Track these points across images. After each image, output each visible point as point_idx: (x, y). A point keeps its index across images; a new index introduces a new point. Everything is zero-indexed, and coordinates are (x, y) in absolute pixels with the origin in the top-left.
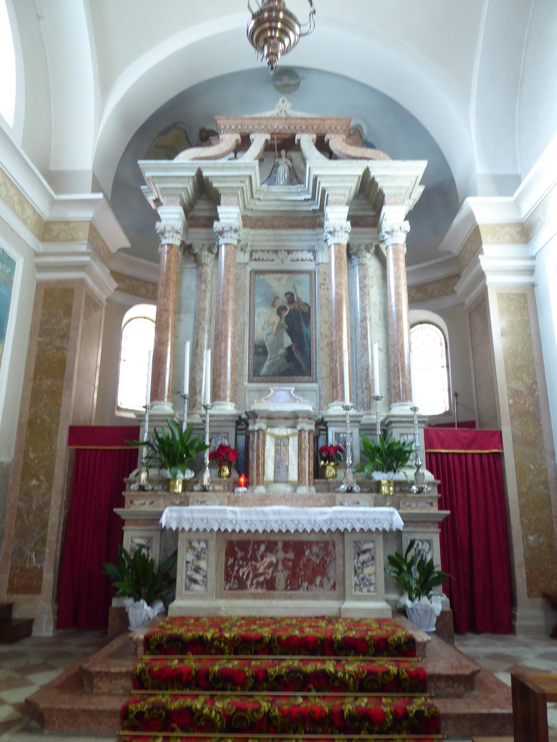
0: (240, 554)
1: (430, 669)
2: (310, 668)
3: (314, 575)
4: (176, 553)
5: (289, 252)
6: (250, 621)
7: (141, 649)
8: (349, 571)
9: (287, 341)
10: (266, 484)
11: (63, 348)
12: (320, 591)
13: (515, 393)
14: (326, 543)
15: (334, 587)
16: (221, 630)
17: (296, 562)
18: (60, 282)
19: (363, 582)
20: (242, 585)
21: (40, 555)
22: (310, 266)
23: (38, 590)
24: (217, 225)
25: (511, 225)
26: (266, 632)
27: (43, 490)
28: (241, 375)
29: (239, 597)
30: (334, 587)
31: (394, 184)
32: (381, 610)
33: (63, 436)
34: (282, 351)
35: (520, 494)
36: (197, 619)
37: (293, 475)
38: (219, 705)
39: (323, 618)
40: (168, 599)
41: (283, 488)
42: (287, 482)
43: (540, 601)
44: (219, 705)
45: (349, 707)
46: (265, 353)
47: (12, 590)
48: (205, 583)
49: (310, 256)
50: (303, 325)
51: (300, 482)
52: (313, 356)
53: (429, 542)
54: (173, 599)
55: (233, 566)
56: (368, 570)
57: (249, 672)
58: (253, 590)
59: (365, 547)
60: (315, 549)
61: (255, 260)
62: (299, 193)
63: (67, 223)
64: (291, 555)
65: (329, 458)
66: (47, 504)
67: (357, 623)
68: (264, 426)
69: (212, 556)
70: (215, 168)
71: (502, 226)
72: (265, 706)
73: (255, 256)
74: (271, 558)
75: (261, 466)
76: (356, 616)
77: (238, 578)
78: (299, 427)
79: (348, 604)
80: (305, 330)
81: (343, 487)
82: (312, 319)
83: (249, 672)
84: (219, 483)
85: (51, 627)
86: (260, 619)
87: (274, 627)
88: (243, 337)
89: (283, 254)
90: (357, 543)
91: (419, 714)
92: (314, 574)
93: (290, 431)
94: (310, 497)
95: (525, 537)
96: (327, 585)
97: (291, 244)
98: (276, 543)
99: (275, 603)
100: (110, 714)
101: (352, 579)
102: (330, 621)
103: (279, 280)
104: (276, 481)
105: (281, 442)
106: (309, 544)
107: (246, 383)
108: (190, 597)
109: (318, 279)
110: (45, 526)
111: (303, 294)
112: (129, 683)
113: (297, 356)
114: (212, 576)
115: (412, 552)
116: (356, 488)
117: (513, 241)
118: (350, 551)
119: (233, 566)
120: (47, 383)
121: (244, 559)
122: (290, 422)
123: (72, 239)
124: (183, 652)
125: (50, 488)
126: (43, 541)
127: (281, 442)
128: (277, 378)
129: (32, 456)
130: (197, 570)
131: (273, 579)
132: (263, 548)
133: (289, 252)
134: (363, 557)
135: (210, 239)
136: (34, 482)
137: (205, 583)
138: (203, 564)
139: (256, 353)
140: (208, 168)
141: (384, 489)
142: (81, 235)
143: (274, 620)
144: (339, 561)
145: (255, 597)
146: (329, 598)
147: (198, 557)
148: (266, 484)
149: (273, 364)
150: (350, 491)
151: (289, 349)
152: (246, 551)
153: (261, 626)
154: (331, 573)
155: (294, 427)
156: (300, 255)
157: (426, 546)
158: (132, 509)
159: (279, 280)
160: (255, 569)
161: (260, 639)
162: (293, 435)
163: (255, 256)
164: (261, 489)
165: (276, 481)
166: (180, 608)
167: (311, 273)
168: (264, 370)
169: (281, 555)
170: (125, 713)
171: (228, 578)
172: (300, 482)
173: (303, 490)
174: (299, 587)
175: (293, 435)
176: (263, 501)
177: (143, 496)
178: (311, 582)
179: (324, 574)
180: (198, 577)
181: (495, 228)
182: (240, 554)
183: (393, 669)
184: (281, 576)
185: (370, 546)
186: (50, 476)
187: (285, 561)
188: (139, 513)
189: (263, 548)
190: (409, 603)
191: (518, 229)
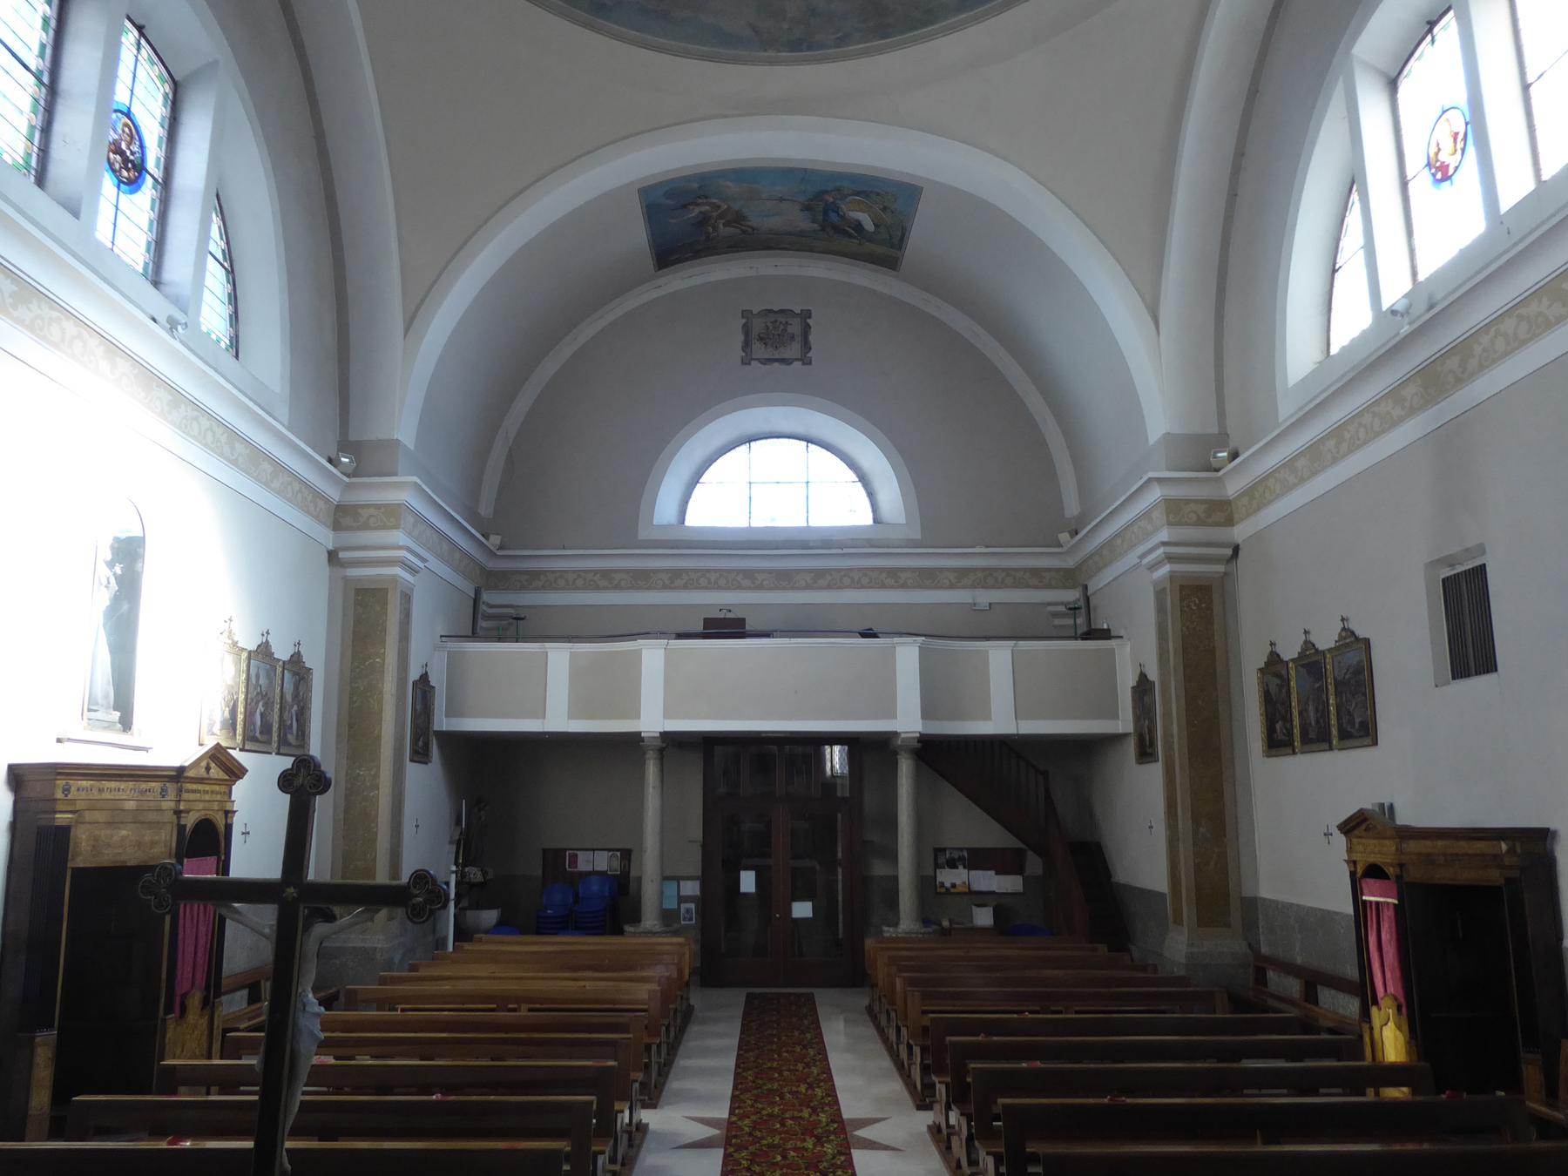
87: (752, 1149)
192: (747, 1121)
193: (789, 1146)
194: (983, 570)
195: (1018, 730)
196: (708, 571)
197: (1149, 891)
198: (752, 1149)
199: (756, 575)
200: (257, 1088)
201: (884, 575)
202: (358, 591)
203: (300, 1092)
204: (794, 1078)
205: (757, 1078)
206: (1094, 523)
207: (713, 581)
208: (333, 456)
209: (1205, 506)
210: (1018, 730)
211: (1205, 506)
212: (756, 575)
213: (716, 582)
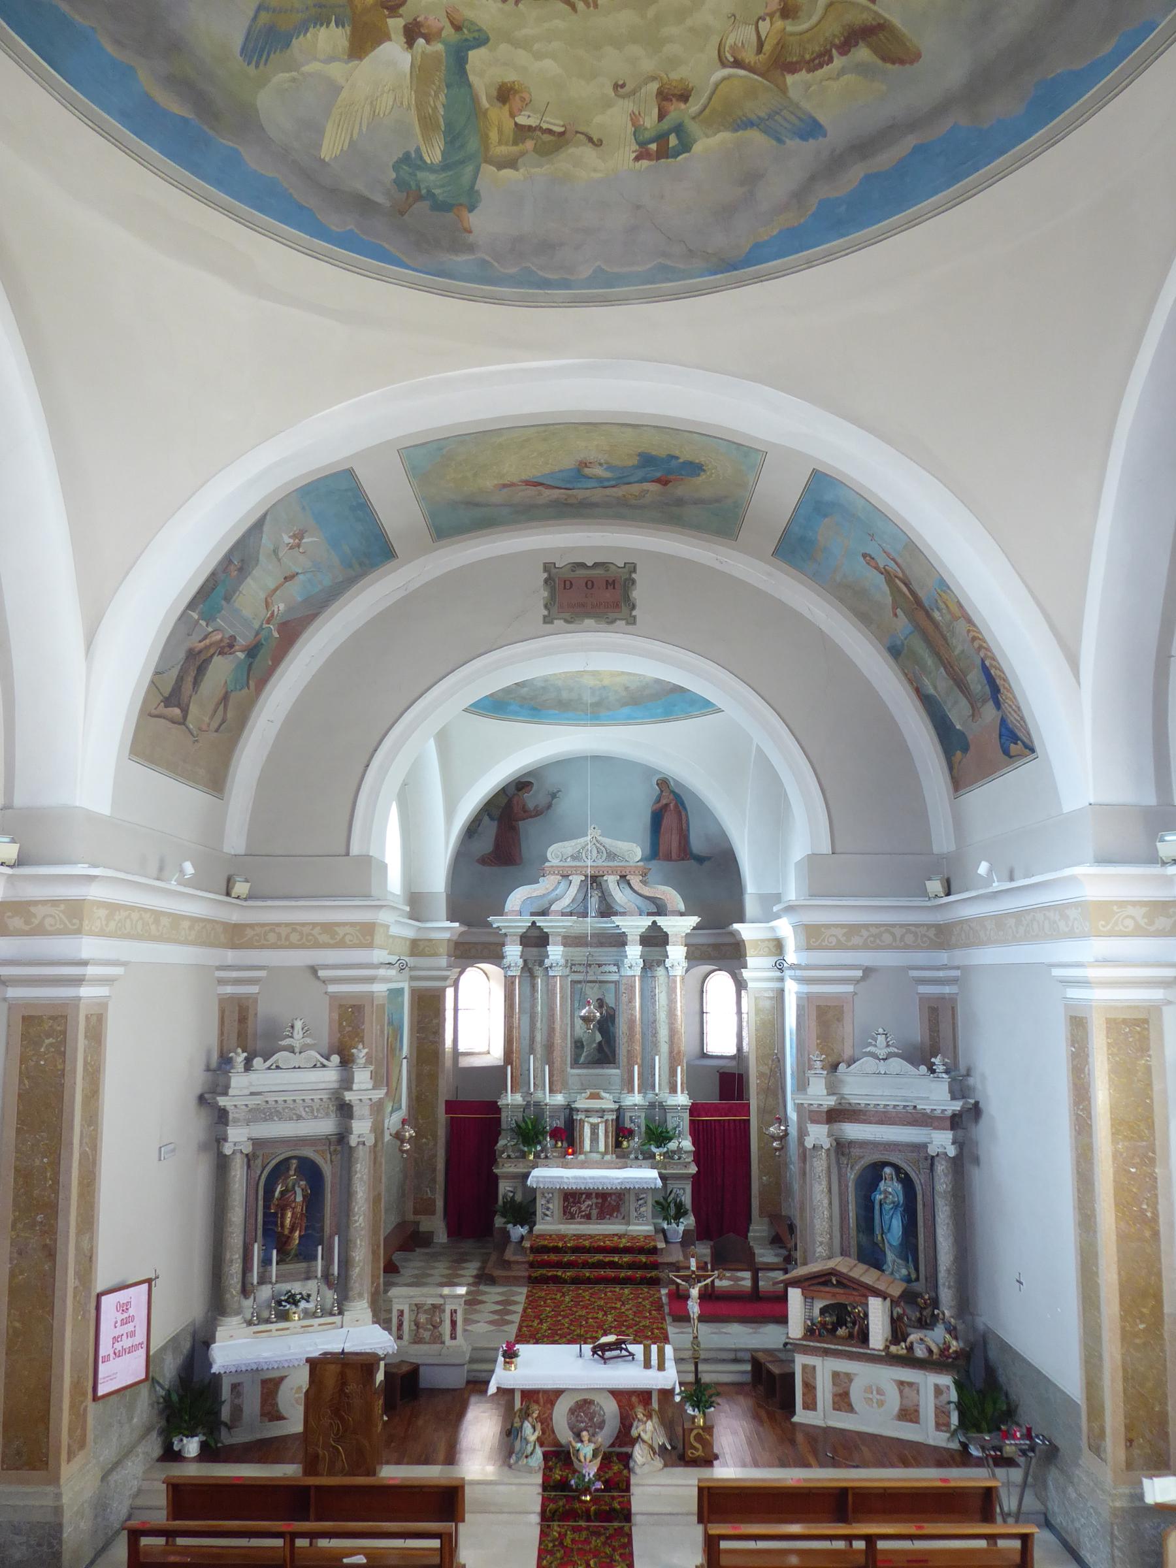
0: (571, 1200)
1: (660, 1260)
2: (607, 1259)
3: (613, 1212)
4: (535, 1199)
5: (600, 966)
6: (579, 1237)
7: (528, 1251)
8: (632, 1209)
9: (599, 1037)
10: (585, 1153)
11: (436, 1042)
12: (617, 1220)
13: (761, 1075)
14: (620, 1194)
15: (624, 1218)
16: (565, 1242)
17: (603, 1205)
18: (427, 990)
19: (641, 1216)
20: (573, 1217)
21: (433, 1190)
22: (615, 977)
23: (433, 1213)
24: (547, 962)
25: (769, 940)
26: (587, 1243)
27: (432, 1144)
28: (566, 1064)
29: (571, 1224)
30: (624, 1218)
31: (674, 929)
32: (648, 1231)
33: (442, 1108)
34: (595, 1045)
35: (760, 1149)
36: (550, 1236)
37: (602, 1148)
38: (568, 1274)
39: (616, 1235)
40: (532, 1224)
41: (596, 1157)
42: (598, 1152)
43: (766, 1220)
44: (568, 1274)
45: (622, 1275)
46: (582, 1046)
47: (416, 1213)
48: (552, 1216)
49: (615, 969)
50: (610, 1024)
51: (606, 1152)
52: (617, 1049)
53: (684, 1189)
54: (535, 1225)
55: (567, 1207)
56: (642, 1209)
57: (580, 1261)
58: (579, 1220)
59: (642, 1196)
60: (613, 1197)
61: (574, 972)
62: (606, 923)
63: (430, 940)
64: (600, 1201)
65: (625, 1137)
66: (435, 1156)
67: (633, 1238)
68: (583, 1117)
69: (556, 1202)
70: (546, 921)
71: (763, 941)
72: (587, 1275)
73: (574, 968)
74: (589, 1202)
75: (582, 1142)
76: (635, 1234)
77: (570, 1213)
78: (605, 1118)
79: (631, 1228)
80: (612, 1028)
81: (632, 1156)
82: (617, 1020)
83: (580, 1261)
84: (556, 1152)
85: (446, 1236)
86: (584, 1235)
87: (571, 1317)
88: (566, 1036)
89: (594, 968)
90: (637, 1195)
91: (651, 1277)
92: (613, 1211)
93: (599, 1120)
94: (612, 1162)
95: (760, 1178)
96: (620, 1217)
97: (601, 958)
98: (591, 1194)
99: (591, 1227)
100: (524, 1277)
101: (634, 1214)
102: (620, 1237)
103: (592, 988)
104: (591, 1152)
105: (594, 1128)
106: (610, 1194)
107: (569, 1069)
108: (544, 1223)
109: (622, 988)
110: (434, 1170)
111: (610, 1000)
112: (527, 1266)
113: (606, 1049)
114: (556, 1212)
115: (672, 1195)
116: (640, 1157)
117: (770, 954)
118: (633, 1198)
119: (567, 1207)
120: (426, 1068)
121: (573, 1202)
122: (600, 1114)
123: (435, 955)
124: (548, 1252)
125: (435, 1145)
126: (434, 1180)
127: (594, 1128)
128: (590, 1066)
129: (421, 1121)
130: (548, 1209)
131: (590, 1214)
132: (584, 1196)
133: (600, 966)
134: (640, 1202)
135: (540, 956)
136: (424, 1140)
137: (552, 1216)
138: (551, 1206)
139: (576, 1047)
140: (539, 921)
141: (657, 1157)
142: (441, 950)
143: (591, 1236)
144: (627, 1204)
145: (580, 1223)
146: (621, 1224)
147: (548, 1202)
148: (585, 1153)
149: (587, 1056)
150: (637, 1158)
151: (600, 1043)
152: (575, 1198)
153: (585, 1240)
154: (622, 1210)
155: (602, 1117)
156: (607, 968)
157: (682, 1192)
158: (504, 1170)
159: (592, 988)
160: (580, 1208)
161: (584, 1247)
162: (602, 1122)
163: (574, 968)
164: (582, 1157)
165: (591, 1152)
166: (539, 1230)
167: (616, 983)
168: (582, 1059)
169: (594, 1200)
170: (530, 1277)
171: (565, 1213)
172: (606, 1152)
173: (608, 1157)
174: (604, 1218)
175: (602, 1122)
176: (583, 1165)
177: (511, 1162)
178: (611, 1215)
179: (618, 1211)
180: (547, 1212)
181: (756, 942)
182: (571, 1200)
183: (644, 1260)
184: (594, 1212)
185: (644, 1196)
186: (435, 1137)
187: (597, 1203)
188: (509, 1173)
189: (584, 1196)
190: (666, 1226)
191: (775, 943)
192: (567, 1320)
193: (590, 1316)
194: (877, 926)
195: (692, 1514)
196: (279, 925)
197: (1017, 1353)
198: (571, 1317)
199: (337, 929)
200: (654, 1348)
201: (317, 930)
202: (28, 1020)
203: (454, 1342)
204: (595, 1325)
205: (571, 1324)
206: (973, 894)
207: (283, 936)
208: (848, 1033)
209: (1144, 910)
210: (692, 1514)
211: (1144, 910)
212: (337, 929)
213: (287, 938)
